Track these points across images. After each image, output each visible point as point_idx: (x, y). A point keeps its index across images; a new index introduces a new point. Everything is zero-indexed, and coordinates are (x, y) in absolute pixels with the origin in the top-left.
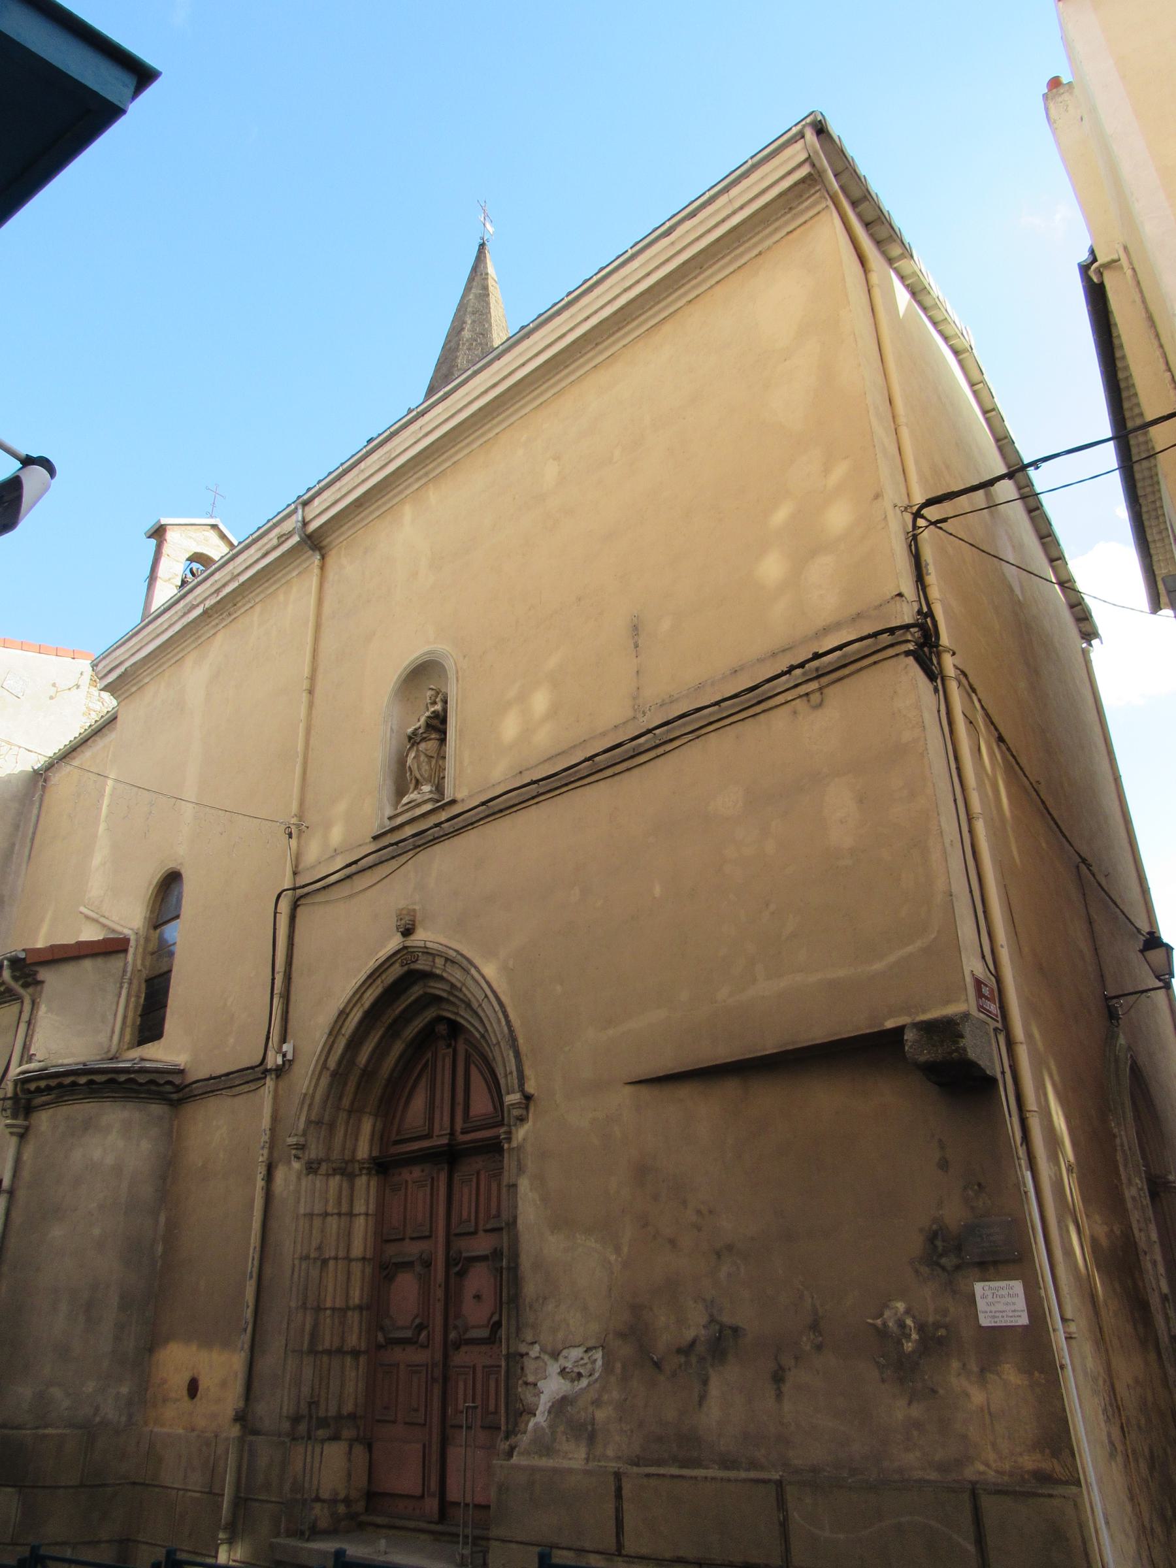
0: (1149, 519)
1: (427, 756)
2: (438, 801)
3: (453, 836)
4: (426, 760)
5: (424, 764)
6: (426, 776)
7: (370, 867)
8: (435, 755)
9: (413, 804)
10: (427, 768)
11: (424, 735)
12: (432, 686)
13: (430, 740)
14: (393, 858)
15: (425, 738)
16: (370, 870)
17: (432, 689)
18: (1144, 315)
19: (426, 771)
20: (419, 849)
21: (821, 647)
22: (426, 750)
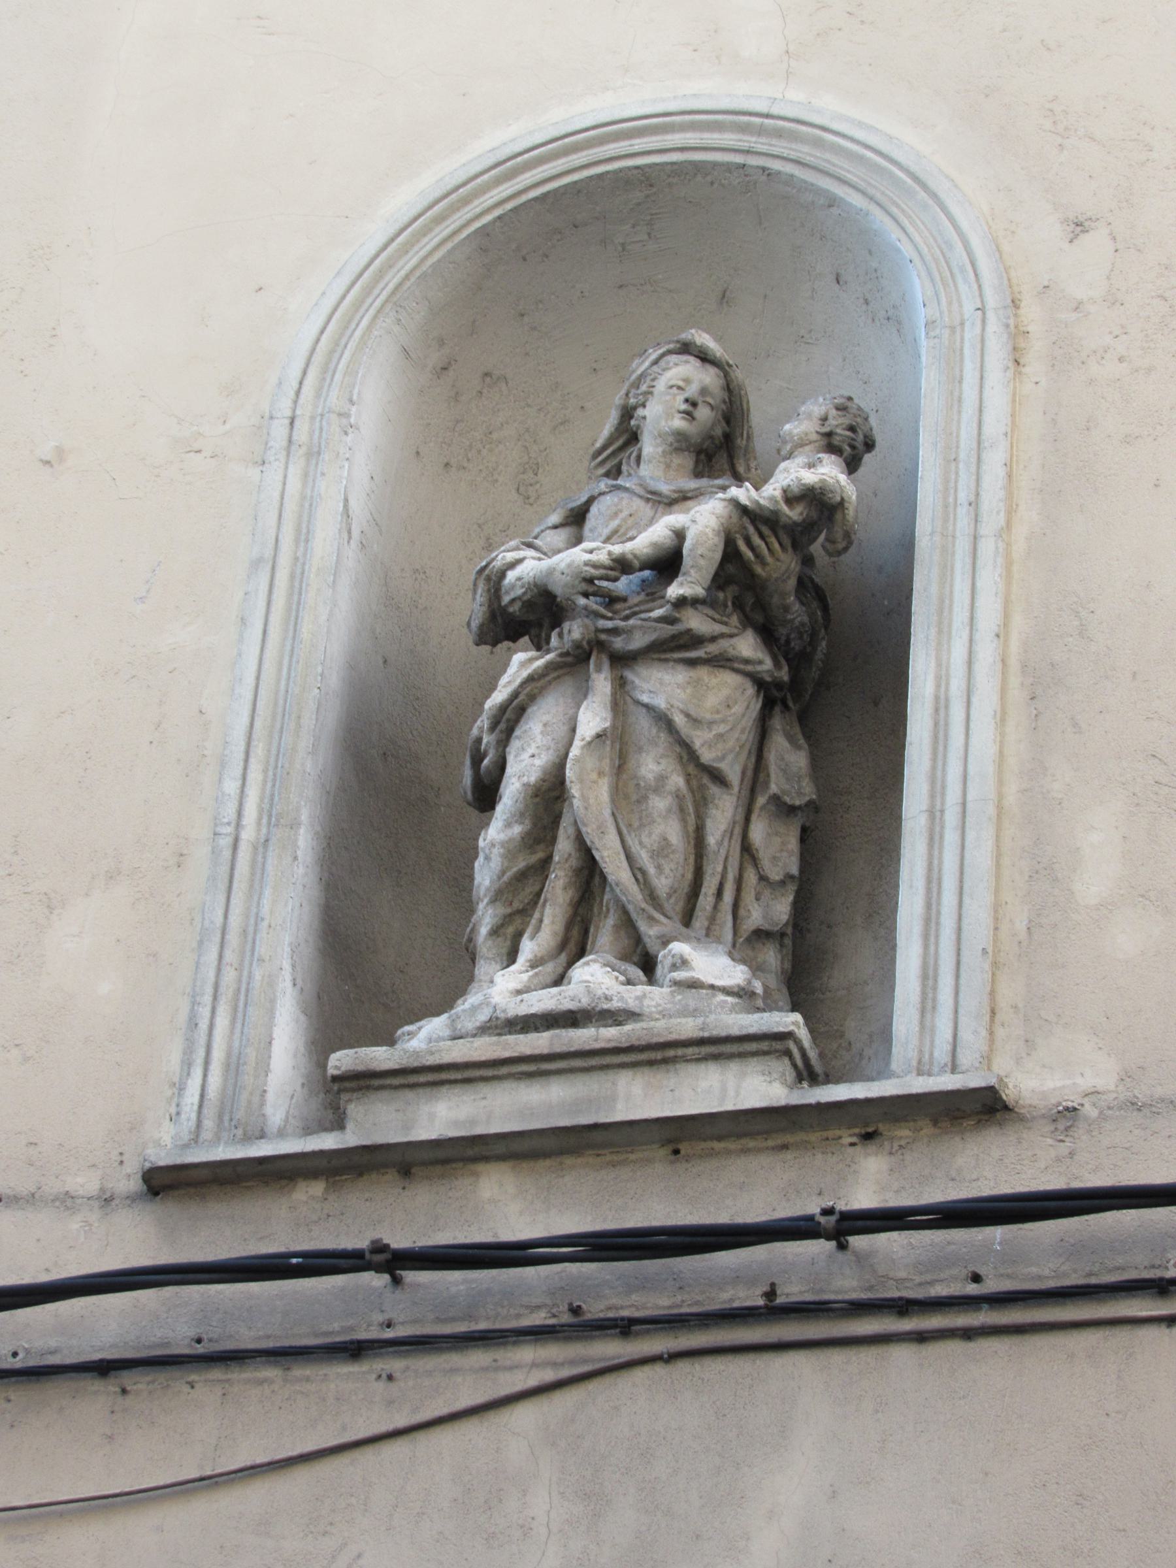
0: (192, 1104)
1: (687, 754)
2: (808, 1075)
3: (968, 1334)
4: (677, 781)
5: (659, 804)
6: (662, 884)
7: (103, 1368)
8: (733, 771)
9: (609, 1035)
10: (674, 832)
11: (696, 622)
12: (704, 339)
13: (722, 662)
14: (355, 1350)
15: (695, 640)
16: (101, 1391)
17: (704, 357)
18: (1163, 1327)
19: (662, 850)
20: (612, 1349)
21: (407, 1128)
22: (695, 721)
